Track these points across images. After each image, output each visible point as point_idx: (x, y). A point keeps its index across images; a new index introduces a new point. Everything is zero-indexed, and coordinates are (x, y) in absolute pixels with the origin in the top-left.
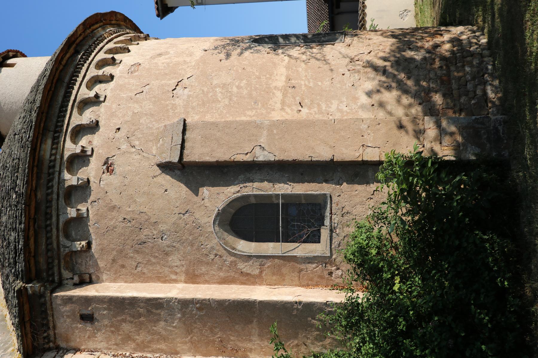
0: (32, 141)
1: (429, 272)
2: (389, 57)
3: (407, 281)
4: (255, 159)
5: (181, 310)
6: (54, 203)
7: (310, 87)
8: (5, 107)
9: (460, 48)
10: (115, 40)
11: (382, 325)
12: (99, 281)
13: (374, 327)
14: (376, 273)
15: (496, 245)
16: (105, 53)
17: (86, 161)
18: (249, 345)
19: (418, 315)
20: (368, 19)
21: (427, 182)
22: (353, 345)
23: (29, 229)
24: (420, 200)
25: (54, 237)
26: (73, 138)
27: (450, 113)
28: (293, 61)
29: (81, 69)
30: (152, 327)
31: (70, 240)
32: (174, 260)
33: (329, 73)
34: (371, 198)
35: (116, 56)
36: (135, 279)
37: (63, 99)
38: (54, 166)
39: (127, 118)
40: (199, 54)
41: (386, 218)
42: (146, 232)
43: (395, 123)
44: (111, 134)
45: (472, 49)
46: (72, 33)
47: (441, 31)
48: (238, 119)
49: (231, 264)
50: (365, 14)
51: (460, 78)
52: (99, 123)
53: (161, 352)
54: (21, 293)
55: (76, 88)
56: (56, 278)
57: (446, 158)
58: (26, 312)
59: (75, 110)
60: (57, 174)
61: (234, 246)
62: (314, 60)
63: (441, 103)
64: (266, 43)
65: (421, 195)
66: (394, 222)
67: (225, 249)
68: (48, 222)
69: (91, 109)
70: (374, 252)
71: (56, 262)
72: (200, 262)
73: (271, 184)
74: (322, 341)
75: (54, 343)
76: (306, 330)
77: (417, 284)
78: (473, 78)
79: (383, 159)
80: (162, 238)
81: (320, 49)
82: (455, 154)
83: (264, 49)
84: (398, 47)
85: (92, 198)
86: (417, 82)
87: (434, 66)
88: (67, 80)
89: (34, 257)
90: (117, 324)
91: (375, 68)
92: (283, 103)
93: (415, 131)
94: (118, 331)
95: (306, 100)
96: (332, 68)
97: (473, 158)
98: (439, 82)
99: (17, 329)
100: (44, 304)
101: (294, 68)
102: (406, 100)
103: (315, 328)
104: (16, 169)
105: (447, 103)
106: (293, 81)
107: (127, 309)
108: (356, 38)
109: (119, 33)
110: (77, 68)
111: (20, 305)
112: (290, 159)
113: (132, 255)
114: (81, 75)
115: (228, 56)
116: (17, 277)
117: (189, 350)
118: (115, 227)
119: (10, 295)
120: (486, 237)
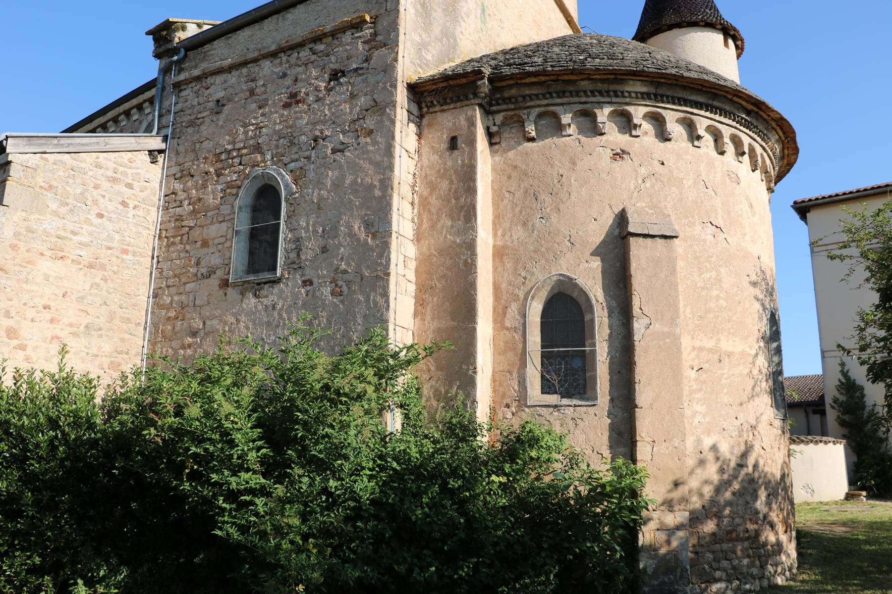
0: (643, 71)
1: (512, 514)
2: (758, 471)
3: (502, 490)
4: (635, 319)
5: (464, 243)
6: (576, 99)
7: (721, 380)
8: (678, 41)
9: (770, 553)
10: (765, 155)
11: (454, 462)
12: (493, 153)
13: (451, 453)
14: (510, 456)
15: (543, 587)
16: (750, 144)
17: (624, 131)
18: (428, 318)
19: (465, 501)
20: (802, 447)
21: (613, 514)
22: (431, 431)
23: (546, 75)
24: (592, 506)
25: (538, 102)
26: (650, 115)
27: (693, 541)
28: (750, 359)
29: (729, 119)
30: (446, 212)
31: (536, 119)
32: (519, 233)
33: (738, 401)
34: (593, 451)
35: (746, 157)
36: (495, 191)
37: (694, 101)
38: (617, 96)
39: (675, 173)
40: (755, 250)
41: (572, 468)
42: (548, 199)
43: (681, 478)
44: (656, 156)
45: (769, 566)
46: (770, 106)
47: (791, 531)
48: (681, 297)
49: (515, 295)
50: (807, 443)
51: (735, 552)
52: (668, 142)
53: (419, 224)
54: (478, 73)
55: (708, 114)
56: (494, 108)
57: (640, 536)
58: (458, 81)
59: (682, 115)
60: (609, 100)
61: (536, 298)
62: (753, 384)
63: (705, 530)
64: (771, 327)
65: (598, 506)
66: (567, 477)
67: (532, 289)
68: (554, 95)
69: (684, 132)
70: (534, 454)
71: (512, 106)
72: (517, 261)
73: (607, 338)
74: (434, 396)
75: (427, 113)
76: (446, 380)
77: (499, 500)
78: (734, 568)
79: (639, 465)
80: (543, 218)
81: (765, 391)
82: (646, 546)
83: (764, 326)
84: (770, 482)
85: (583, 139)
86: (729, 503)
87: (748, 522)
88: (716, 103)
89: (517, 83)
90: (448, 176)
91: (744, 455)
92: (701, 349)
93: (671, 500)
94: (440, 177)
95: (705, 376)
96: (744, 405)
97: (641, 566)
98: (730, 528)
99: (440, 74)
100: (467, 98)
101: (742, 361)
102: (708, 491)
103: (448, 390)
104: (612, 57)
105: (704, 538)
106: (727, 360)
107: (464, 184)
108: (780, 432)
109: (773, 158)
110: (730, 114)
111: (465, 75)
112: (636, 359)
113: (523, 186)
114: (722, 119)
115: (754, 284)
116: (495, 68)
117: (421, 254)
118: (552, 166)
119: (475, 63)
120: (552, 577)
